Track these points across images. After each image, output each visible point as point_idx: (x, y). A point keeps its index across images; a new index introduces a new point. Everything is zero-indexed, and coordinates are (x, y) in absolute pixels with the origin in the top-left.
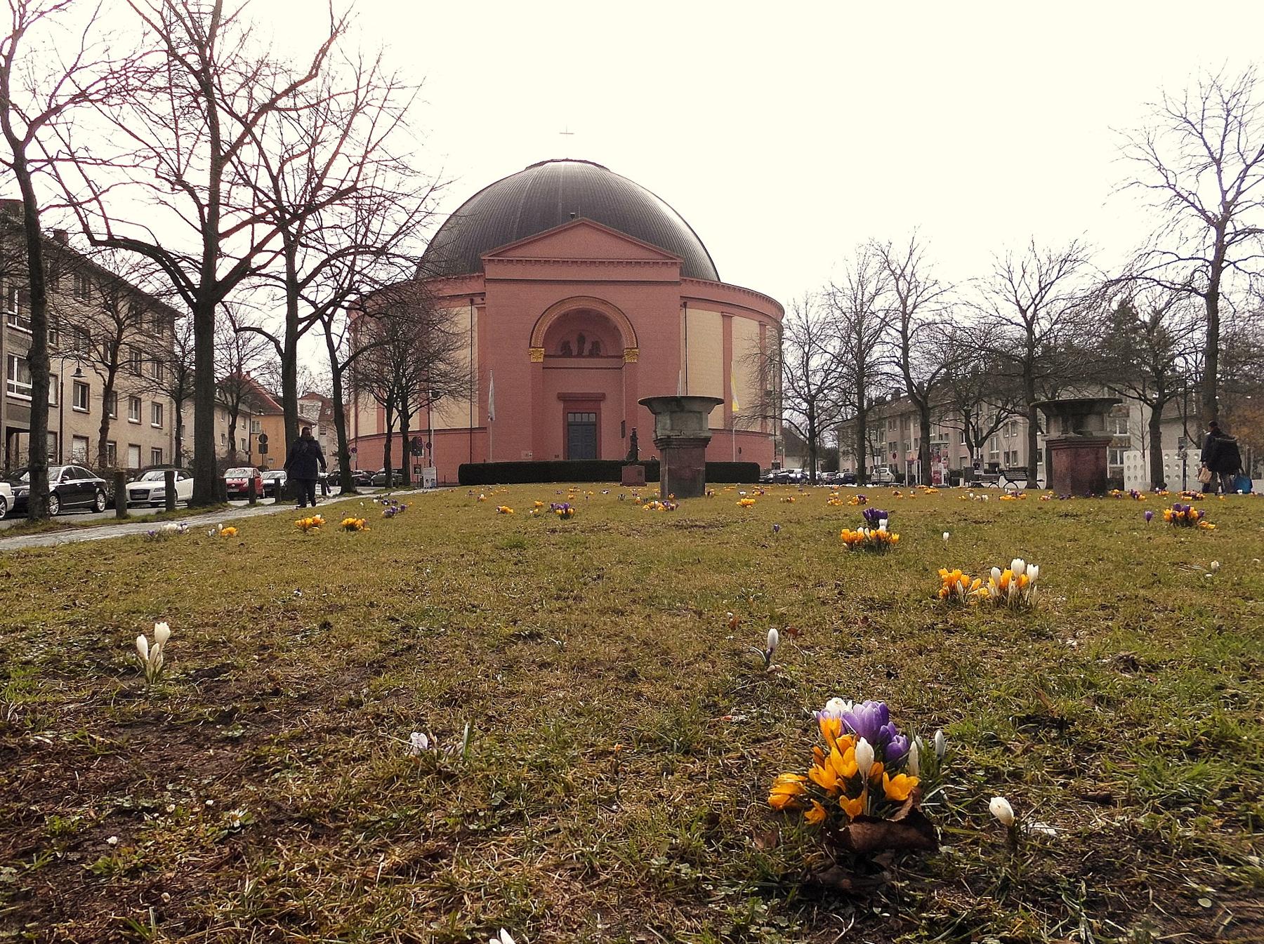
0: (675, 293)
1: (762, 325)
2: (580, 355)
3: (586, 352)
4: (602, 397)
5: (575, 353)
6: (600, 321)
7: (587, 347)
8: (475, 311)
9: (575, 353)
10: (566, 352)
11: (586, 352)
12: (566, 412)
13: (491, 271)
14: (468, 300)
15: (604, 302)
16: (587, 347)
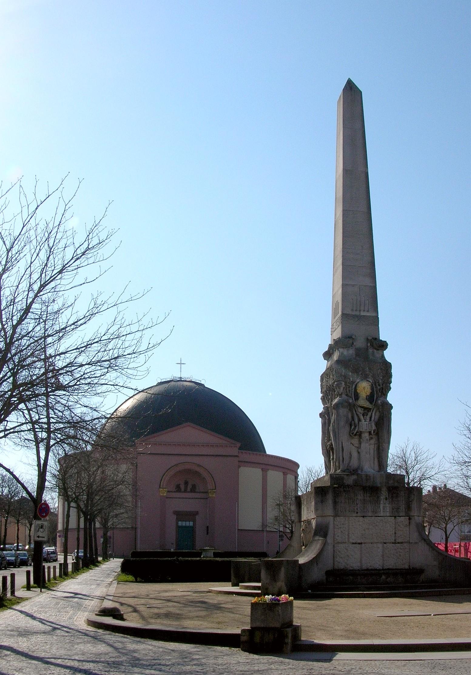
1: (285, 474)
2: (185, 491)
3: (189, 489)
4: (197, 513)
5: (183, 490)
6: (197, 474)
7: (189, 487)
9: (183, 490)
10: (178, 489)
11: (189, 489)
12: (178, 520)
15: (199, 466)
16: (189, 487)
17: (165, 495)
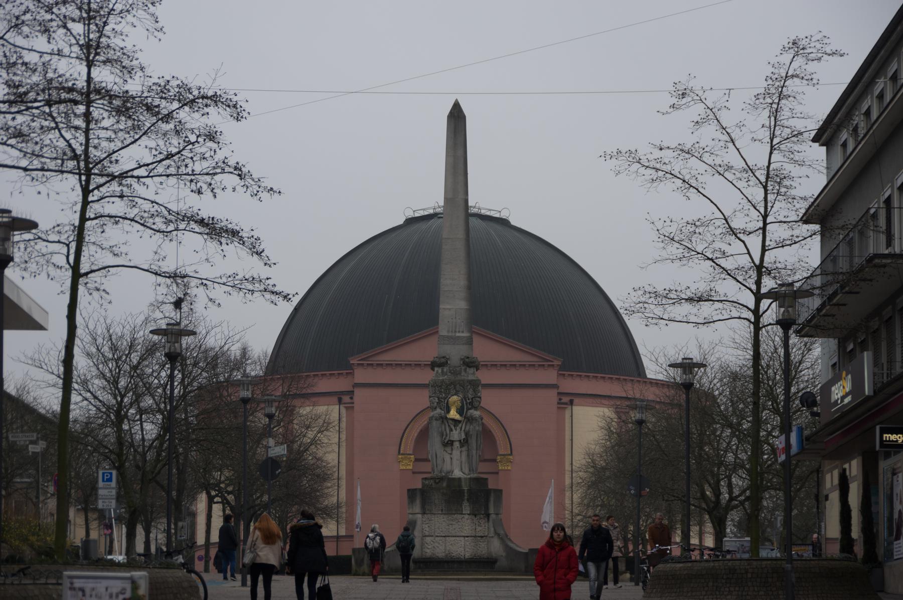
0: (552, 394)
8: (343, 411)
13: (361, 375)
14: (335, 399)
17: (411, 467)
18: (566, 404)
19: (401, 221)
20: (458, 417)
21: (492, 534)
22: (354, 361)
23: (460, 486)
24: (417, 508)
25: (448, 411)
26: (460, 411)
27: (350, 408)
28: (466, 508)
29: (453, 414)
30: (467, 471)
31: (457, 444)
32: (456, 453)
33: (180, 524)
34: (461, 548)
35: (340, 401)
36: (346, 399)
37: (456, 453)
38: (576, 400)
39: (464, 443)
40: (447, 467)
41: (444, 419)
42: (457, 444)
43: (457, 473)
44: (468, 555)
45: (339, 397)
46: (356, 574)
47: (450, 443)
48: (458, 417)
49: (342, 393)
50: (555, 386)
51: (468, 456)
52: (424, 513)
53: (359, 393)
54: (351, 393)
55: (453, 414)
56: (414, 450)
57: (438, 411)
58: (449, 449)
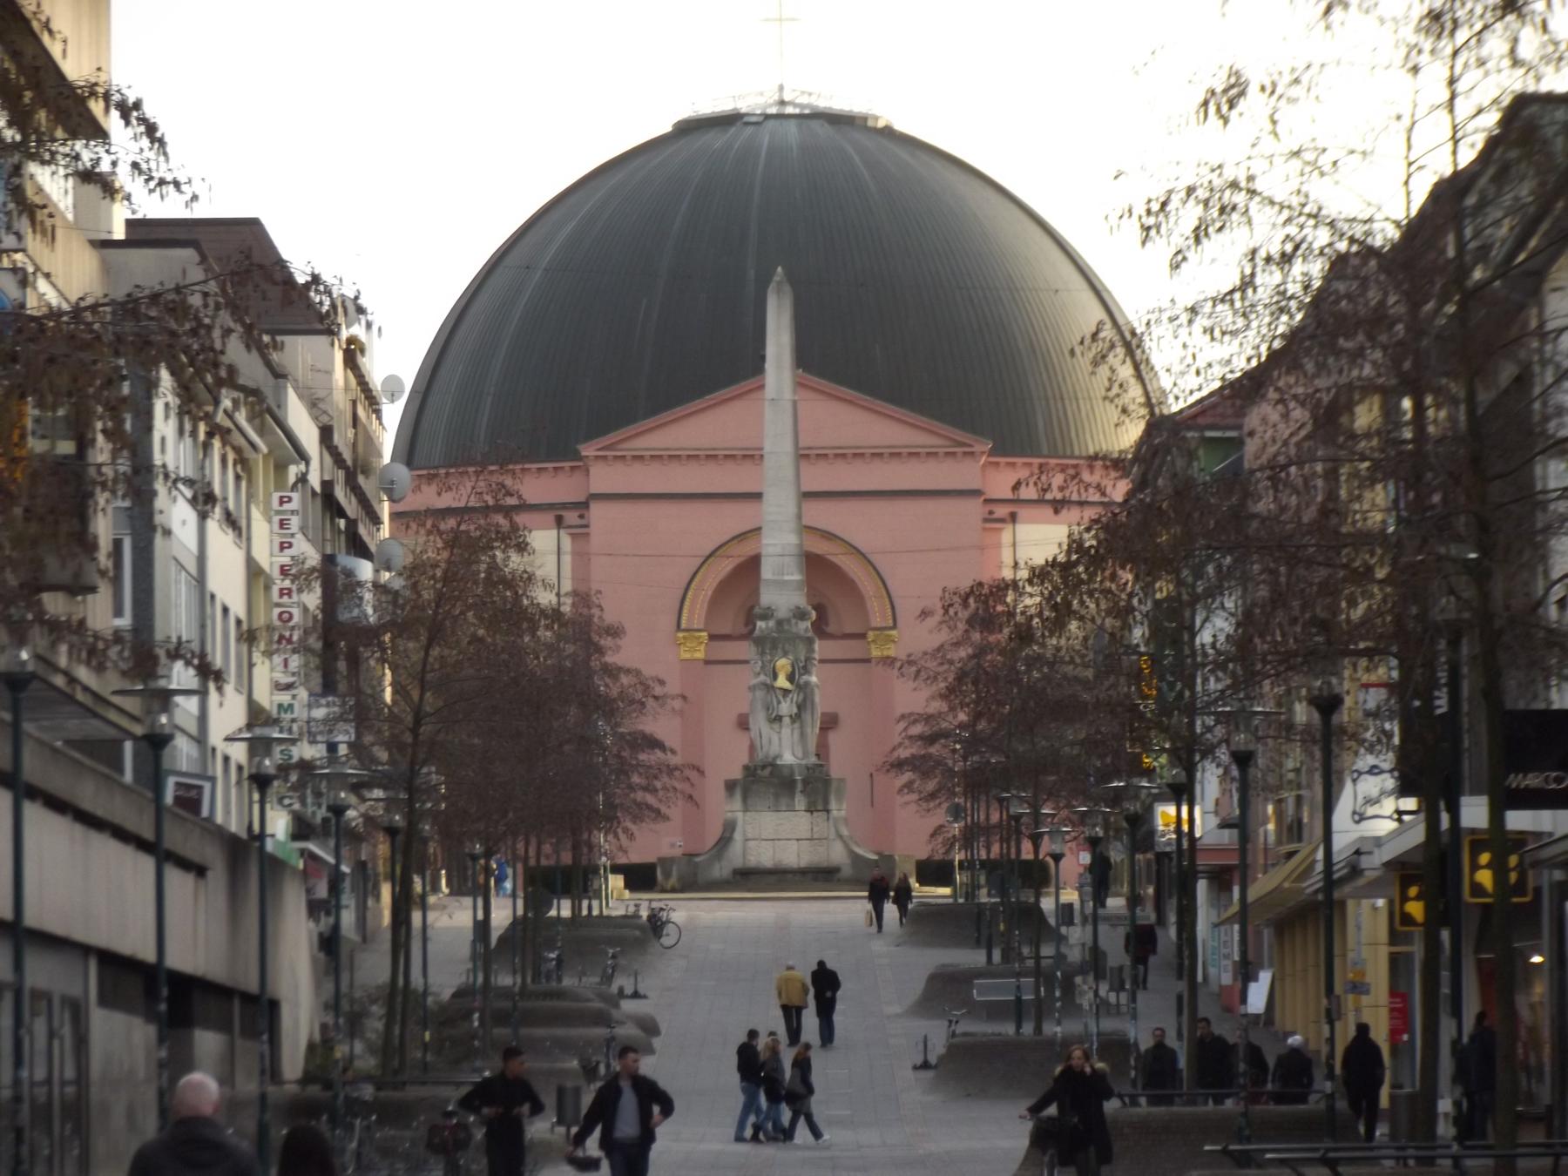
8: (567, 543)
13: (604, 478)
14: (550, 517)
17: (700, 655)
18: (1002, 520)
19: (666, 127)
20: (787, 685)
21: (832, 835)
22: (588, 450)
23: (792, 774)
24: (737, 803)
25: (775, 677)
26: (791, 678)
27: (581, 534)
28: (800, 802)
29: (782, 682)
30: (800, 755)
31: (787, 720)
32: (786, 731)
33: (1411, 1162)
34: (793, 855)
35: (559, 522)
36: (571, 517)
37: (786, 731)
38: (1023, 512)
39: (797, 718)
40: (774, 750)
41: (770, 688)
42: (787, 720)
43: (788, 758)
44: (803, 864)
45: (558, 514)
46: (664, 891)
47: (779, 719)
48: (787, 685)
49: (565, 506)
50: (975, 493)
51: (803, 735)
52: (746, 810)
53: (597, 511)
54: (582, 506)
55: (782, 682)
56: (706, 623)
57: (762, 678)
58: (776, 726)
